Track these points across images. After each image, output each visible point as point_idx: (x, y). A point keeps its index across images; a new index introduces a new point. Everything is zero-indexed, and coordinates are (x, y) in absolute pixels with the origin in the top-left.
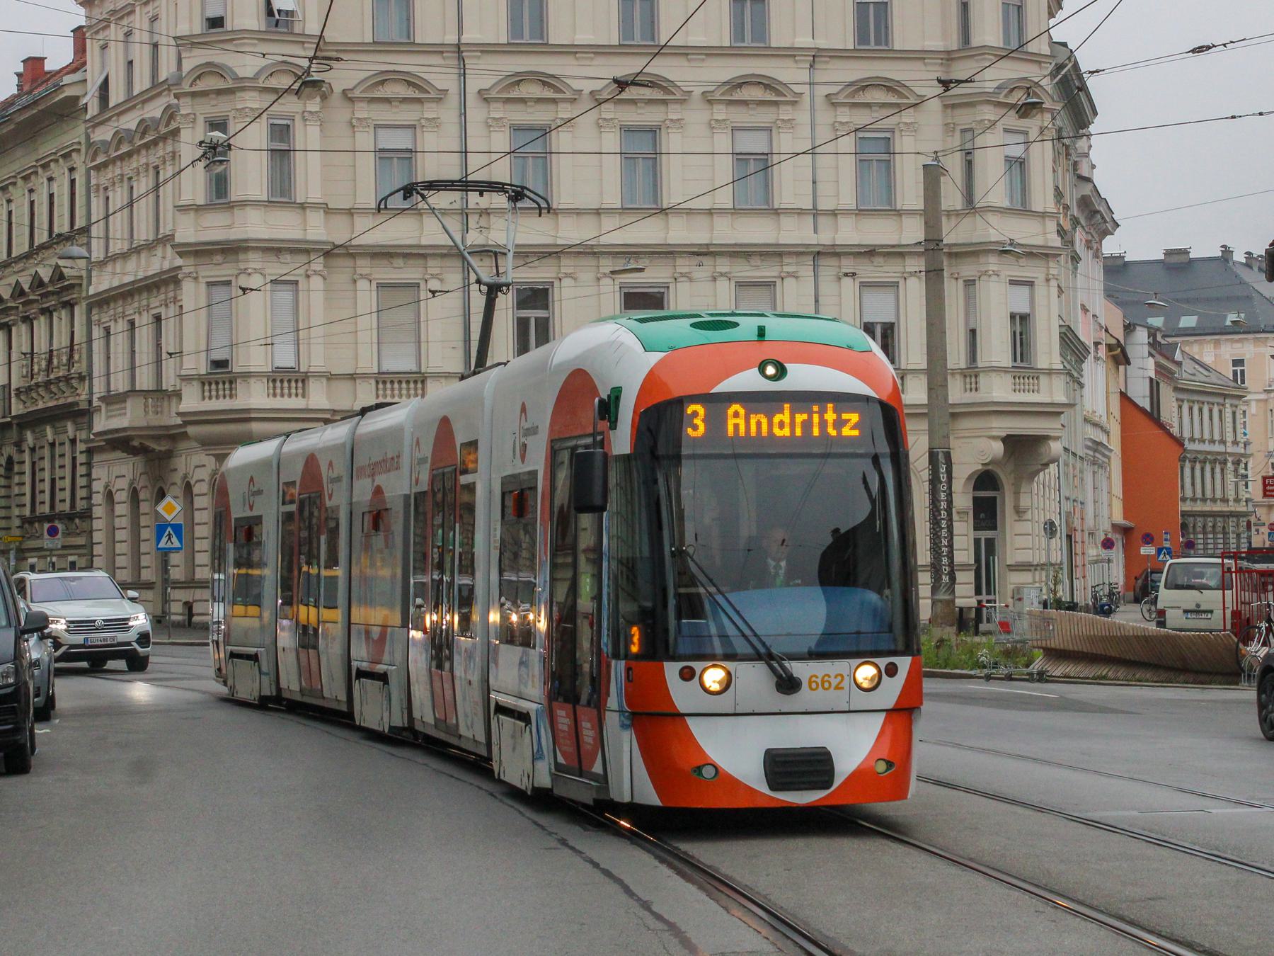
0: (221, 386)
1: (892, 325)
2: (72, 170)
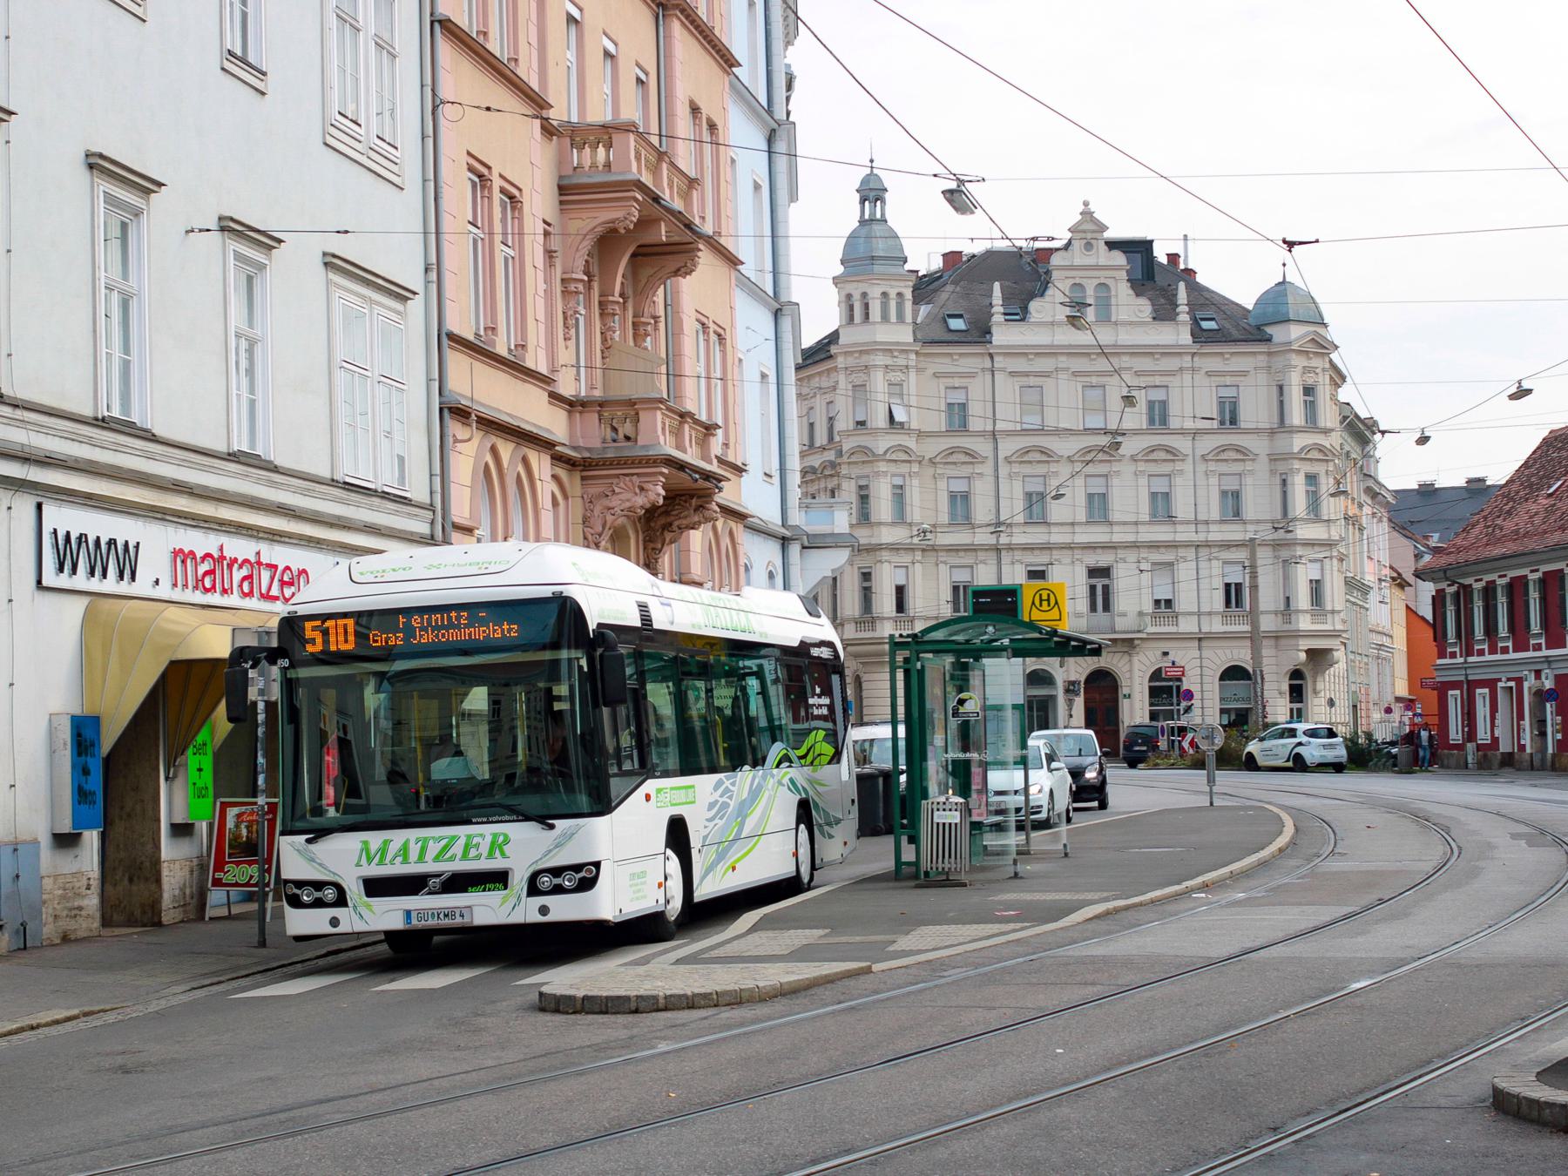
1: (1241, 584)
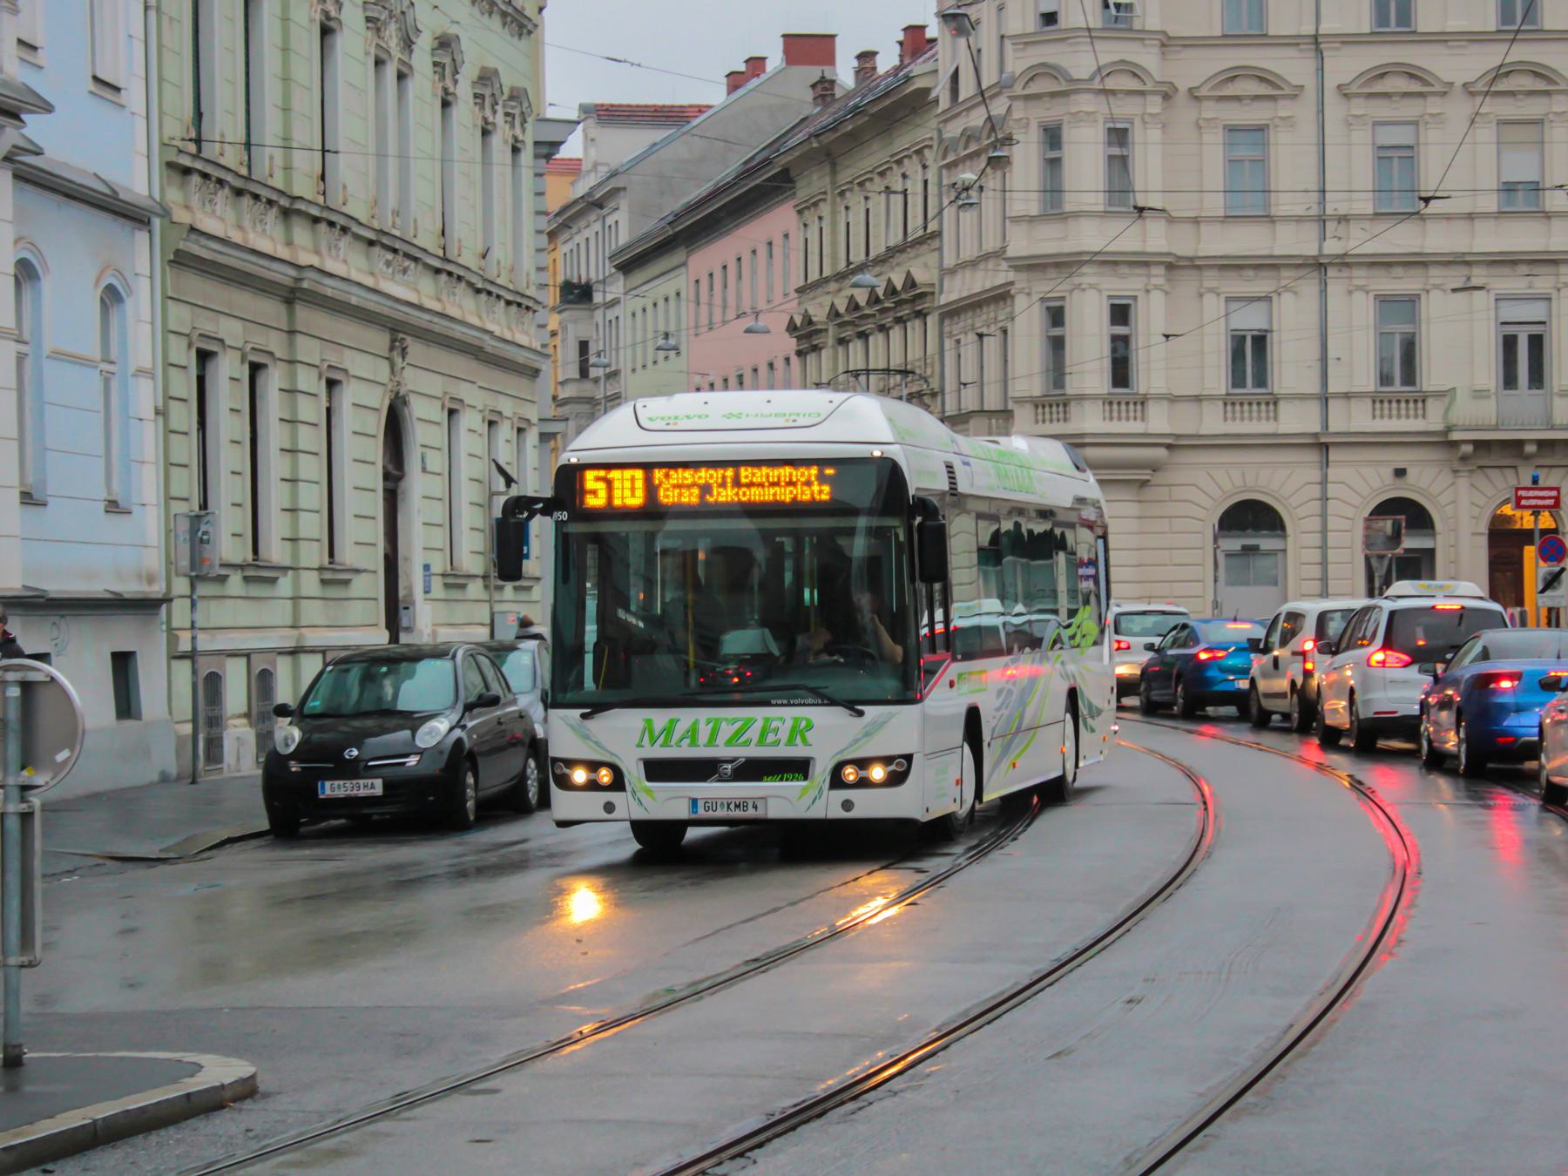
0: (1054, 409)
2: (820, 218)
